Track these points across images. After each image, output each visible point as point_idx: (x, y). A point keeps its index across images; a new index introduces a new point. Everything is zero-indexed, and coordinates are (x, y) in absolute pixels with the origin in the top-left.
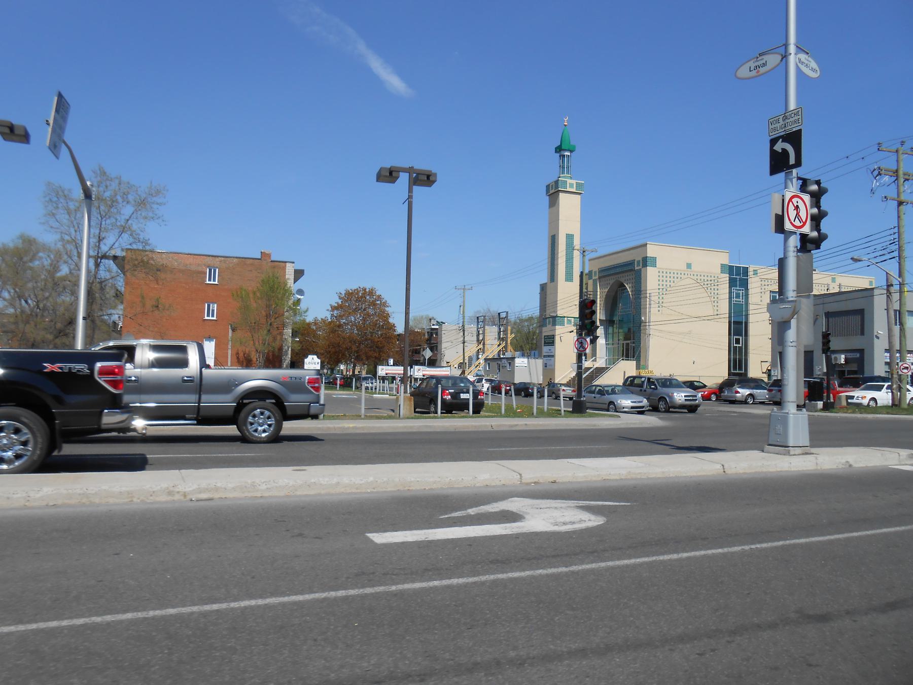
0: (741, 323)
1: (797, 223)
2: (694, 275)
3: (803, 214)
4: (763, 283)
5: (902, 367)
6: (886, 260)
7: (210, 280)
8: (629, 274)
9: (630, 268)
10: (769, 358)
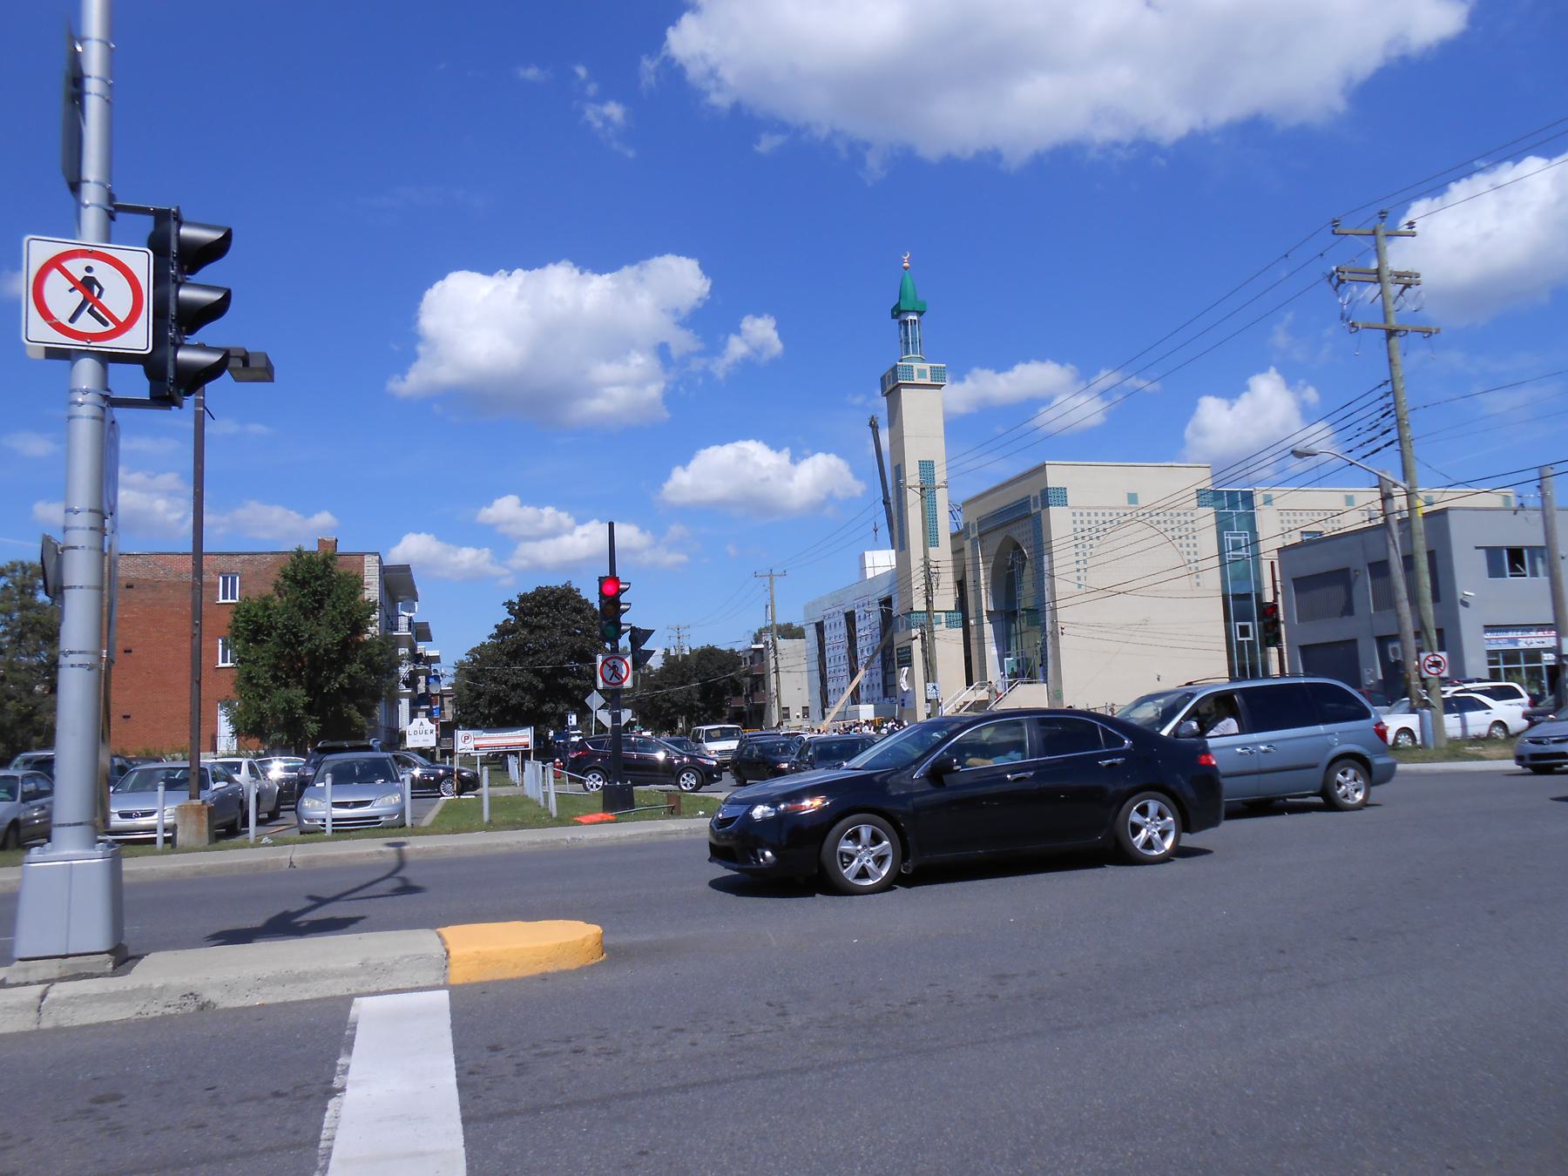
0: (1248, 596)
4: (1285, 518)
5: (1428, 663)
7: (225, 597)
8: (1025, 521)
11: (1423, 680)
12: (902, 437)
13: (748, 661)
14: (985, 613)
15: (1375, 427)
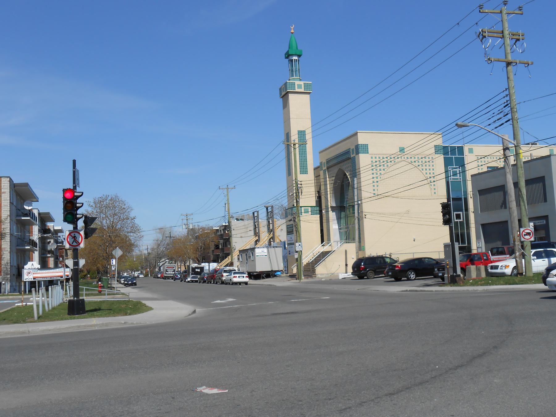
0: (460, 199)
5: (524, 233)
9: (347, 156)
11: (522, 242)
13: (222, 231)
14: (329, 207)
15: (501, 112)
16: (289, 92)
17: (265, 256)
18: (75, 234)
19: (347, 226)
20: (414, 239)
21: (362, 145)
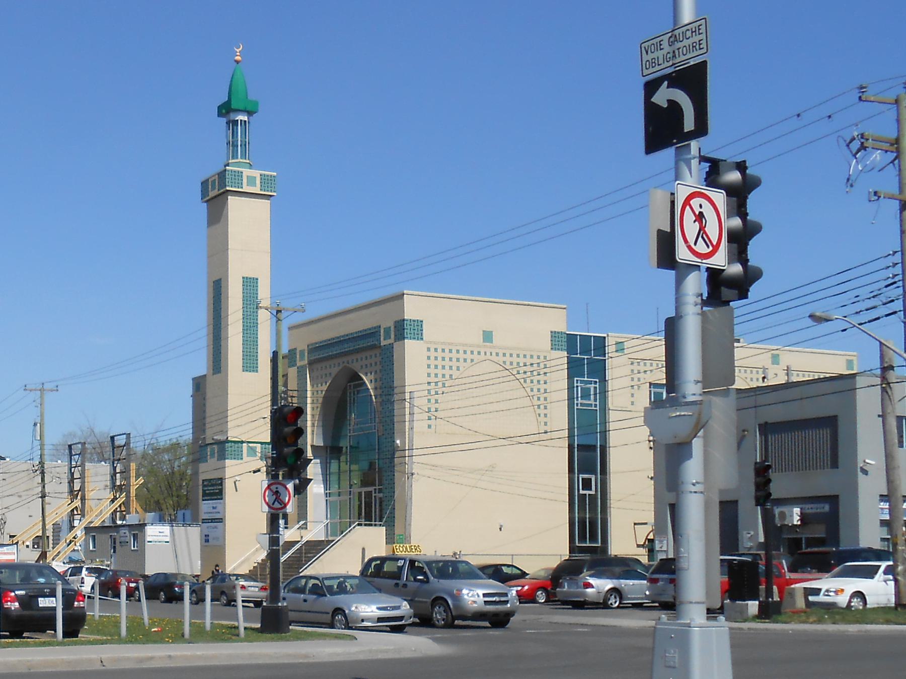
1: (701, 248)
2: (497, 354)
3: (712, 230)
6: (878, 318)
8: (368, 354)
9: (370, 342)
10: (650, 517)
12: (226, 249)
16: (230, 193)
17: (166, 542)
18: (277, 488)
19: (328, 491)
20: (501, 526)
21: (412, 322)
